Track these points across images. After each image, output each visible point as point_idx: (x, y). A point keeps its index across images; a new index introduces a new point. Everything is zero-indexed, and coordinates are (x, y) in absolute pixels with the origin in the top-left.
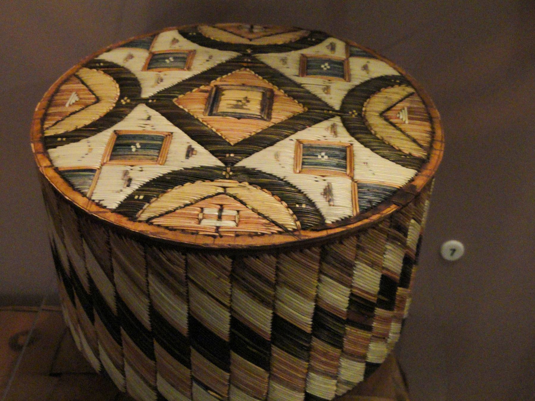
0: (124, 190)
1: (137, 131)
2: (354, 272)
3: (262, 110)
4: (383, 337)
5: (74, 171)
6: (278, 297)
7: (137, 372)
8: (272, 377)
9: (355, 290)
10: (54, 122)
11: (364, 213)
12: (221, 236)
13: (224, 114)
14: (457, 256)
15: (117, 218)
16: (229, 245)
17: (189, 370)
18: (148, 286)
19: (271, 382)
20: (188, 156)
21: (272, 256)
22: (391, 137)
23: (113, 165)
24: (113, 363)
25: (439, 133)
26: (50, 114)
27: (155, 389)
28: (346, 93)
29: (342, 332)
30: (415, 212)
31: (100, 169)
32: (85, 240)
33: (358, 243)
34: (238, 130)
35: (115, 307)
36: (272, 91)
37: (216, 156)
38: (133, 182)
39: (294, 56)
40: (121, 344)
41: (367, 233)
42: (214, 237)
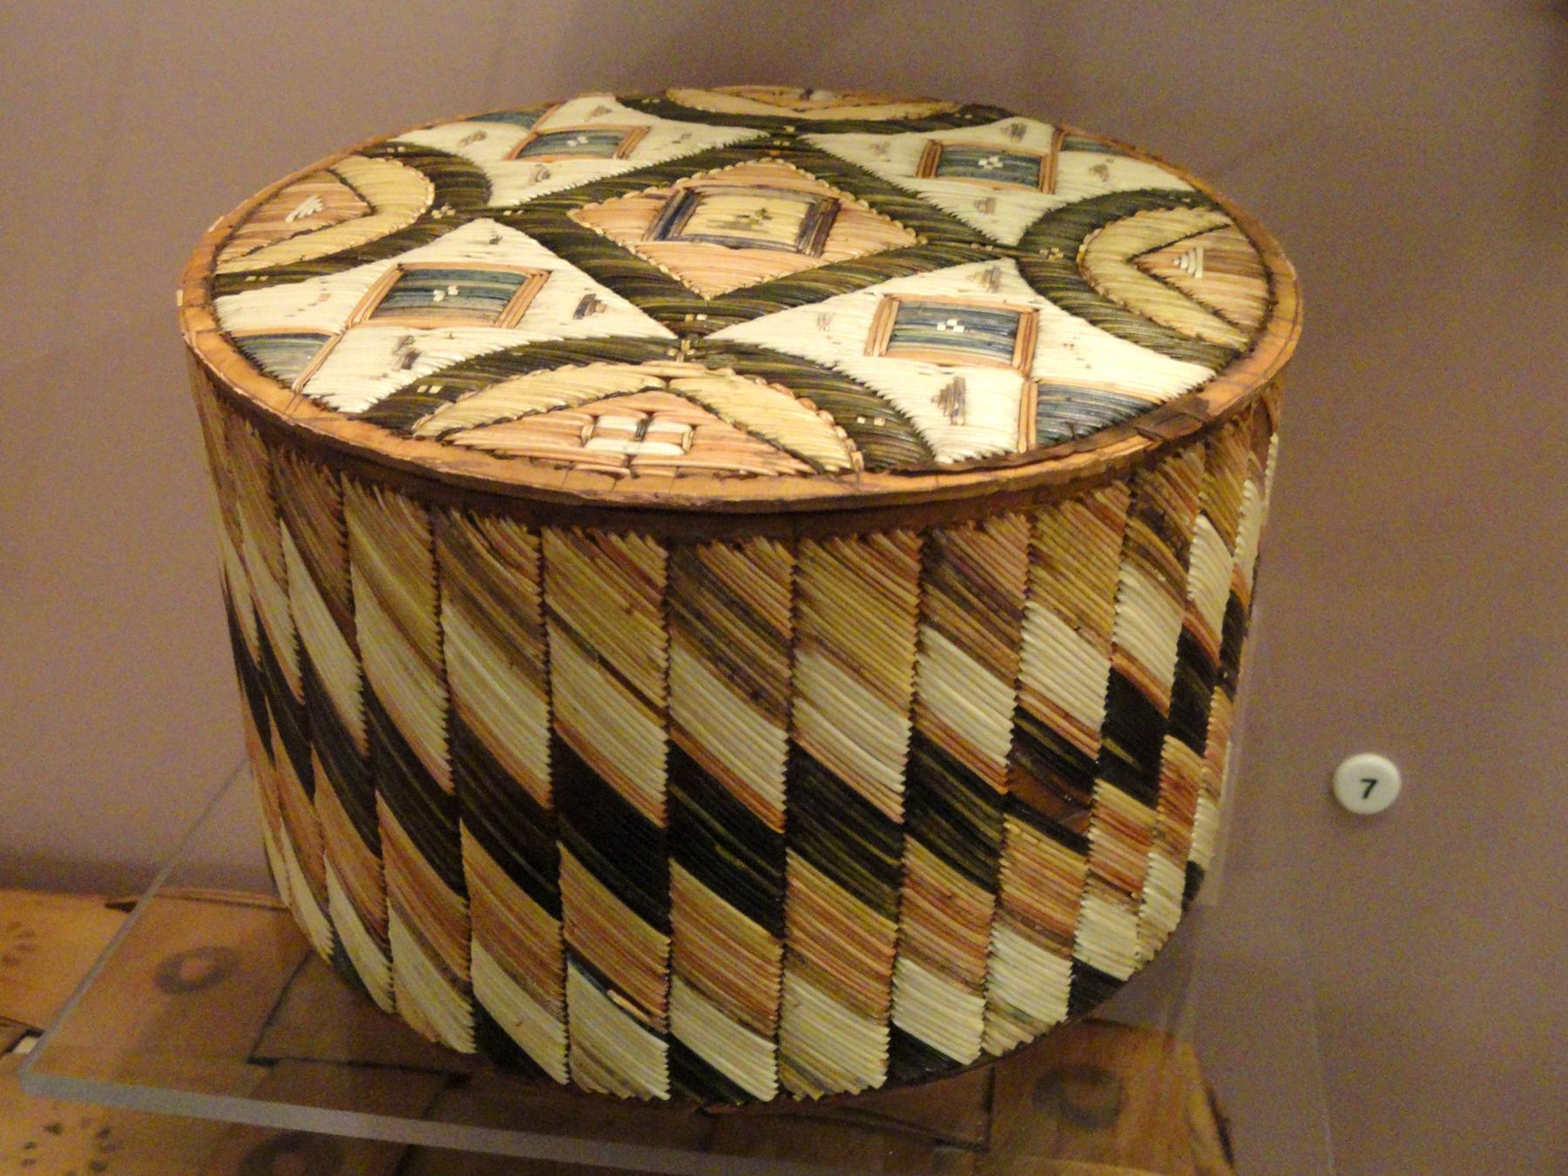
0: (391, 374)
1: (456, 264)
2: (1026, 636)
4: (1128, 891)
5: (276, 336)
6: (800, 686)
8: (790, 959)
9: (1028, 699)
10: (247, 250)
12: (636, 476)
14: (1380, 801)
15: (358, 431)
17: (557, 923)
18: (441, 643)
19: (790, 977)
20: (580, 312)
21: (780, 548)
22: (1147, 301)
24: (357, 909)
25: (1289, 303)
26: (239, 237)
27: (467, 990)
28: (1039, 215)
29: (993, 834)
30: (1209, 494)
31: (340, 337)
32: (288, 525)
33: (1034, 542)
34: (729, 271)
35: (362, 726)
36: (836, 201)
37: (657, 319)
38: (419, 360)
39: (910, 145)
40: (378, 852)
41: (1059, 511)
42: (617, 476)
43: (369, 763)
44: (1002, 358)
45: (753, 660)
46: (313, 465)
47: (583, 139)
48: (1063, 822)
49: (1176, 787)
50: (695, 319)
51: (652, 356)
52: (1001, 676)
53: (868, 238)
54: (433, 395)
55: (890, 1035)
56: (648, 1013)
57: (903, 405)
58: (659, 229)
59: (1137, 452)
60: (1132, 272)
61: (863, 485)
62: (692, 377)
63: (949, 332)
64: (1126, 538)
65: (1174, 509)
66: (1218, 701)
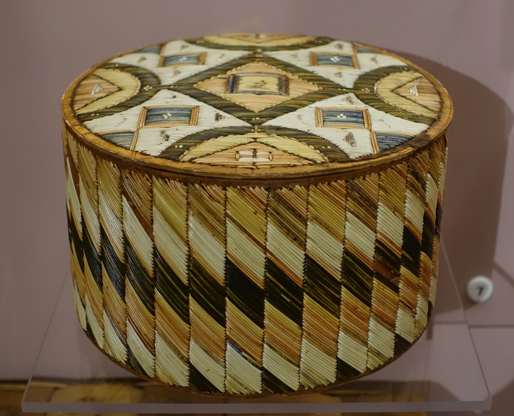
3: (280, 88)
4: (410, 307)
7: (169, 343)
10: (83, 105)
11: (383, 152)
12: (258, 169)
13: (244, 92)
14: (487, 295)
15: (161, 161)
16: (267, 173)
23: (149, 128)
25: (448, 103)
28: (357, 77)
39: (304, 53)
42: (252, 169)
43: (154, 279)
44: (361, 125)
45: (295, 227)
46: (141, 174)
47: (185, 58)
48: (392, 281)
49: (425, 270)
50: (256, 119)
51: (247, 132)
52: (371, 229)
53: (303, 89)
54: (181, 148)
55: (337, 362)
56: (255, 359)
57: (334, 142)
58: (230, 90)
59: (410, 152)
60: (394, 95)
61: (330, 166)
62: (263, 137)
63: (341, 118)
64: (407, 181)
65: (421, 171)
66: (435, 241)
